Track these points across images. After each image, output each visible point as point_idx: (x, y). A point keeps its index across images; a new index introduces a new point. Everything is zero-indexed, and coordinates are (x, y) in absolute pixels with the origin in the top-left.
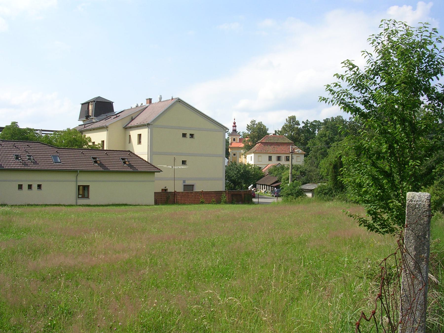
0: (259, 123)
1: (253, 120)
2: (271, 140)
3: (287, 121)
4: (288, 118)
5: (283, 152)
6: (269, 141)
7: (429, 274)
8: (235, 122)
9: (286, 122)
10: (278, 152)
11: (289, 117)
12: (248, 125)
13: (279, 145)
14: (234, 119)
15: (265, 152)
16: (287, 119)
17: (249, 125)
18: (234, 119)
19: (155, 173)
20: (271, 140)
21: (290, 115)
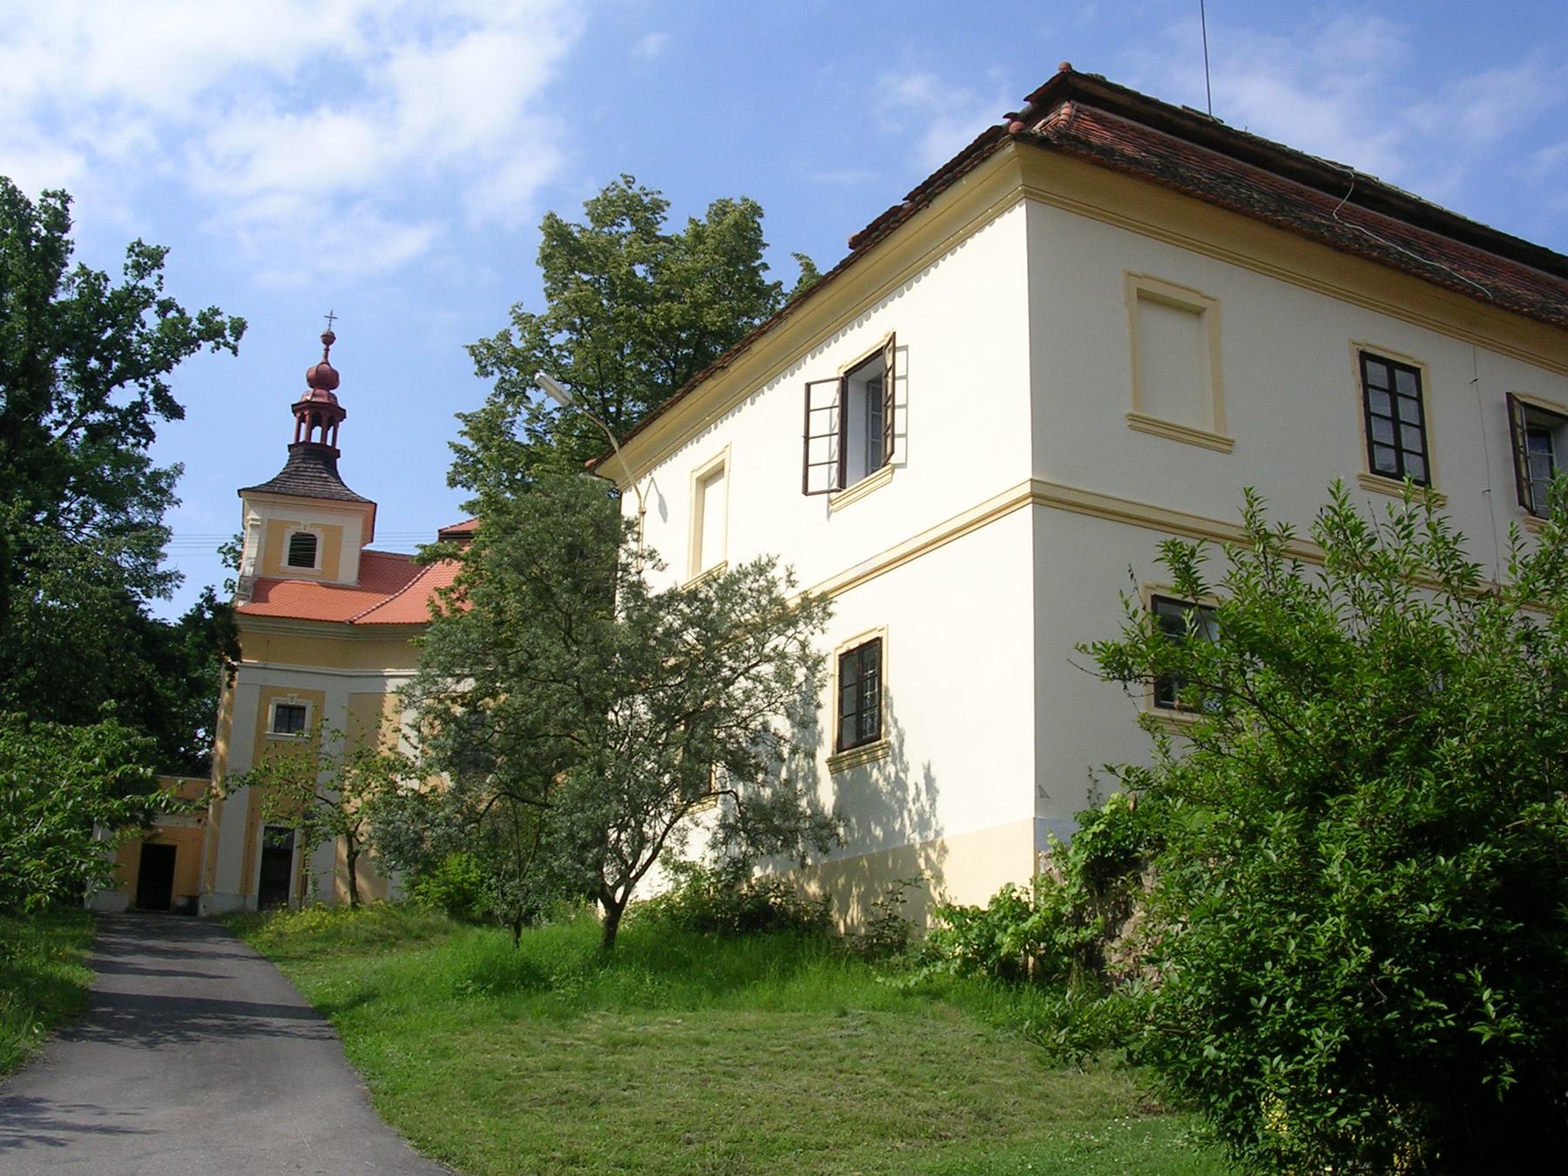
8: (334, 364)
14: (329, 339)
18: (329, 339)
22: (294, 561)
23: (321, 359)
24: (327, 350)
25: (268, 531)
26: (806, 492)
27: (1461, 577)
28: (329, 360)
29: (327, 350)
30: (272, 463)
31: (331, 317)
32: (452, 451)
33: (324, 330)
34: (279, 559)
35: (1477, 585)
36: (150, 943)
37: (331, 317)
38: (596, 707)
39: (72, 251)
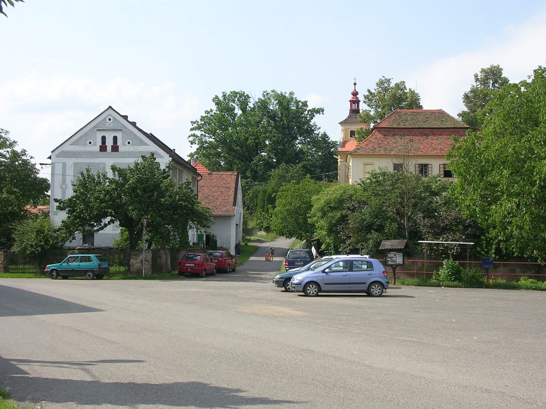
0: (397, 85)
1: (384, 79)
2: (407, 120)
3: (477, 80)
4: (479, 74)
5: (434, 153)
6: (399, 124)
7: (219, 113)
8: (357, 90)
9: (475, 84)
10: (419, 153)
11: (483, 71)
12: (369, 91)
13: (426, 135)
14: (355, 84)
15: (383, 152)
16: (476, 76)
17: (373, 91)
18: (355, 84)
19: (51, 163)
20: (407, 120)
21: (487, 66)
22: (351, 136)
23: (354, 89)
24: (355, 87)
25: (345, 131)
26: (110, 107)
27: (485, 390)
28: (356, 89)
29: (355, 87)
30: (346, 114)
31: (355, 79)
32: (317, 107)
33: (354, 82)
34: (348, 137)
35: (95, 256)
36: (240, 192)
37: (355, 79)
38: (478, 226)
39: (493, 65)
